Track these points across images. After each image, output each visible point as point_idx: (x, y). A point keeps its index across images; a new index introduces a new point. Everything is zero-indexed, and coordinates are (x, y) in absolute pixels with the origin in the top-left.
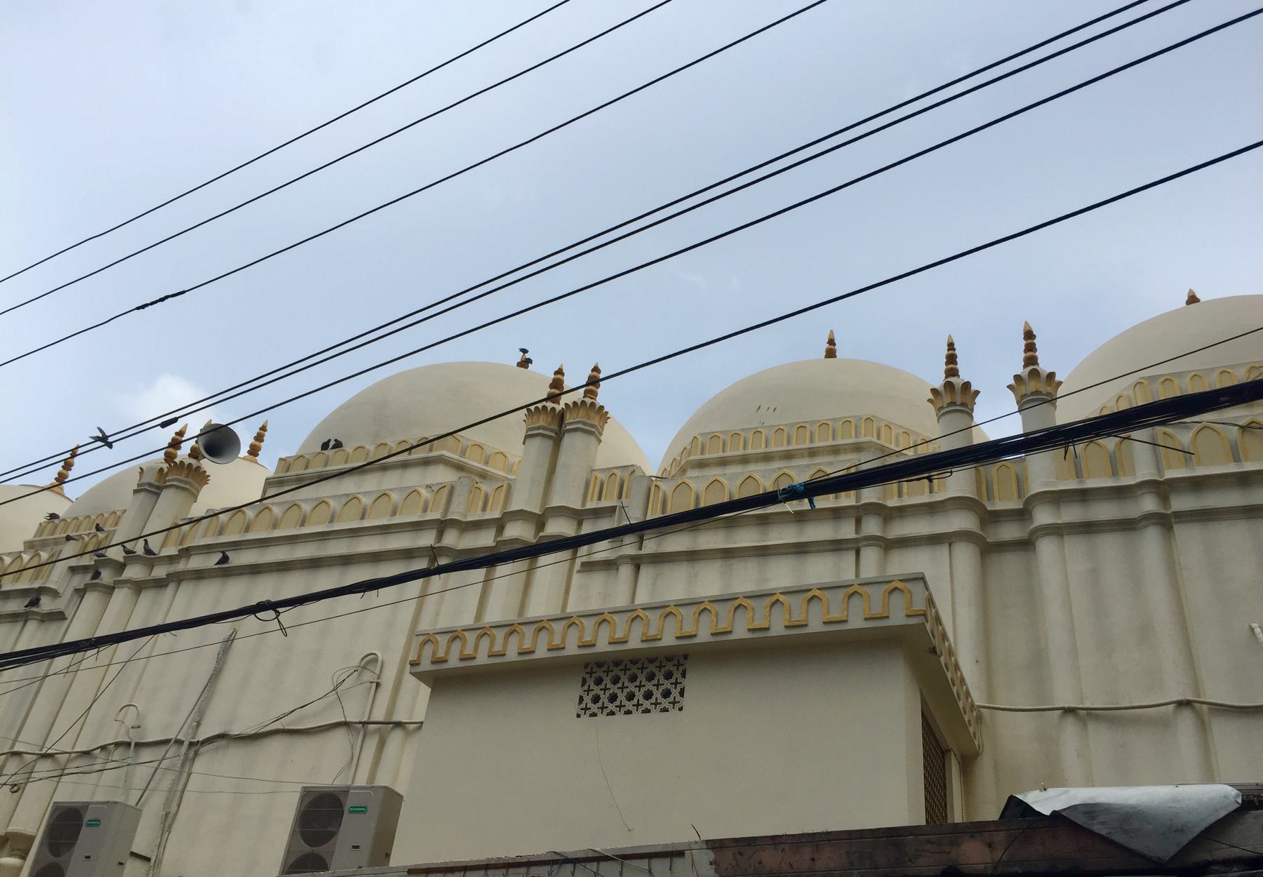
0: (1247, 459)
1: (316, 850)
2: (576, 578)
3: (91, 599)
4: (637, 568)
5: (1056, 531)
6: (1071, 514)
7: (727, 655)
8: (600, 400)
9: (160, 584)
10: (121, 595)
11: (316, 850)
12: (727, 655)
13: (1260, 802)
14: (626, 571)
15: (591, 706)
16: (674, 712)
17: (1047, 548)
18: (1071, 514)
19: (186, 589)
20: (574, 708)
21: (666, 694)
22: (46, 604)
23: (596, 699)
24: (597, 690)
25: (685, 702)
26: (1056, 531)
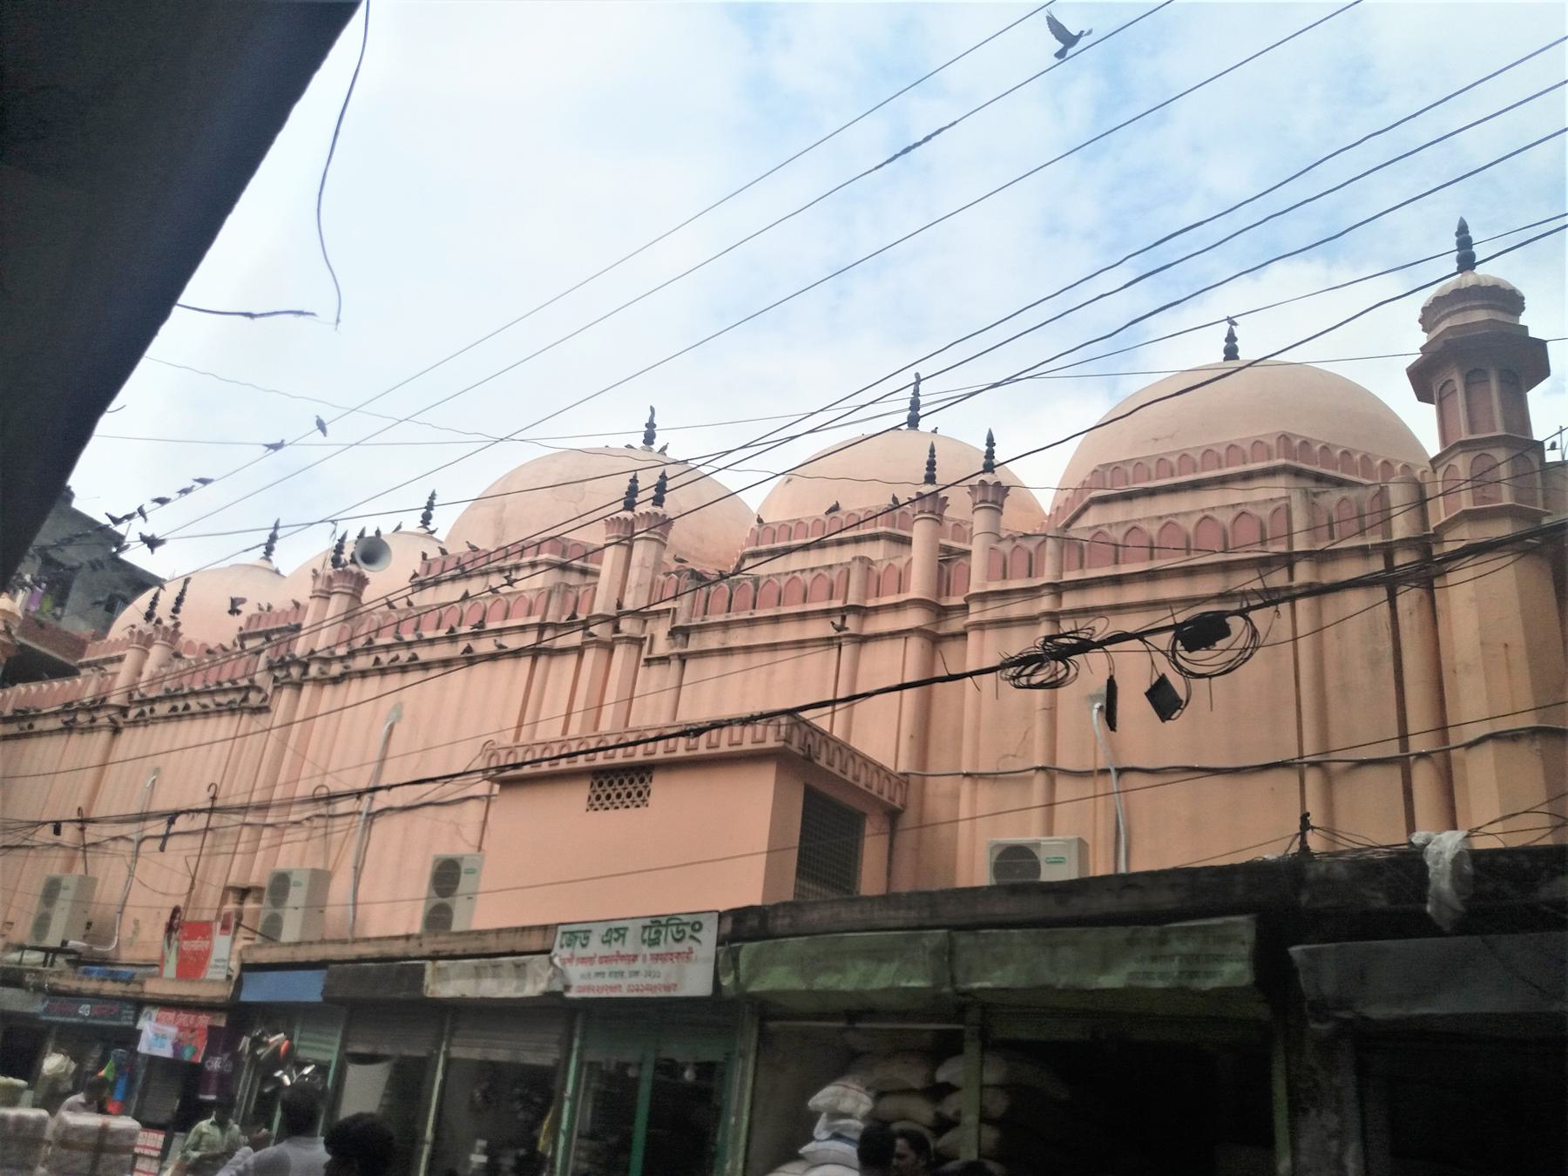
0: (1125, 562)
1: (445, 900)
2: (641, 670)
3: (286, 693)
4: (684, 663)
5: (980, 626)
6: (993, 612)
7: (672, 765)
8: (265, 883)
9: (336, 681)
10: (307, 690)
11: (440, 900)
12: (672, 765)
13: (23, 1063)
14: (675, 664)
15: (597, 802)
16: (642, 808)
17: (973, 637)
18: (993, 612)
19: (356, 684)
20: (584, 803)
21: (640, 794)
22: (254, 699)
23: (598, 798)
24: (599, 791)
25: (650, 800)
26: (980, 626)
